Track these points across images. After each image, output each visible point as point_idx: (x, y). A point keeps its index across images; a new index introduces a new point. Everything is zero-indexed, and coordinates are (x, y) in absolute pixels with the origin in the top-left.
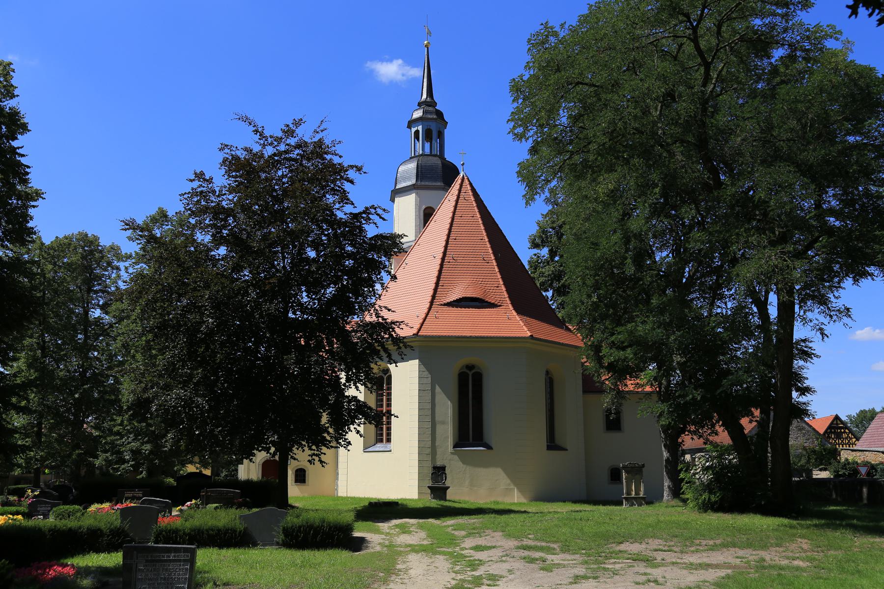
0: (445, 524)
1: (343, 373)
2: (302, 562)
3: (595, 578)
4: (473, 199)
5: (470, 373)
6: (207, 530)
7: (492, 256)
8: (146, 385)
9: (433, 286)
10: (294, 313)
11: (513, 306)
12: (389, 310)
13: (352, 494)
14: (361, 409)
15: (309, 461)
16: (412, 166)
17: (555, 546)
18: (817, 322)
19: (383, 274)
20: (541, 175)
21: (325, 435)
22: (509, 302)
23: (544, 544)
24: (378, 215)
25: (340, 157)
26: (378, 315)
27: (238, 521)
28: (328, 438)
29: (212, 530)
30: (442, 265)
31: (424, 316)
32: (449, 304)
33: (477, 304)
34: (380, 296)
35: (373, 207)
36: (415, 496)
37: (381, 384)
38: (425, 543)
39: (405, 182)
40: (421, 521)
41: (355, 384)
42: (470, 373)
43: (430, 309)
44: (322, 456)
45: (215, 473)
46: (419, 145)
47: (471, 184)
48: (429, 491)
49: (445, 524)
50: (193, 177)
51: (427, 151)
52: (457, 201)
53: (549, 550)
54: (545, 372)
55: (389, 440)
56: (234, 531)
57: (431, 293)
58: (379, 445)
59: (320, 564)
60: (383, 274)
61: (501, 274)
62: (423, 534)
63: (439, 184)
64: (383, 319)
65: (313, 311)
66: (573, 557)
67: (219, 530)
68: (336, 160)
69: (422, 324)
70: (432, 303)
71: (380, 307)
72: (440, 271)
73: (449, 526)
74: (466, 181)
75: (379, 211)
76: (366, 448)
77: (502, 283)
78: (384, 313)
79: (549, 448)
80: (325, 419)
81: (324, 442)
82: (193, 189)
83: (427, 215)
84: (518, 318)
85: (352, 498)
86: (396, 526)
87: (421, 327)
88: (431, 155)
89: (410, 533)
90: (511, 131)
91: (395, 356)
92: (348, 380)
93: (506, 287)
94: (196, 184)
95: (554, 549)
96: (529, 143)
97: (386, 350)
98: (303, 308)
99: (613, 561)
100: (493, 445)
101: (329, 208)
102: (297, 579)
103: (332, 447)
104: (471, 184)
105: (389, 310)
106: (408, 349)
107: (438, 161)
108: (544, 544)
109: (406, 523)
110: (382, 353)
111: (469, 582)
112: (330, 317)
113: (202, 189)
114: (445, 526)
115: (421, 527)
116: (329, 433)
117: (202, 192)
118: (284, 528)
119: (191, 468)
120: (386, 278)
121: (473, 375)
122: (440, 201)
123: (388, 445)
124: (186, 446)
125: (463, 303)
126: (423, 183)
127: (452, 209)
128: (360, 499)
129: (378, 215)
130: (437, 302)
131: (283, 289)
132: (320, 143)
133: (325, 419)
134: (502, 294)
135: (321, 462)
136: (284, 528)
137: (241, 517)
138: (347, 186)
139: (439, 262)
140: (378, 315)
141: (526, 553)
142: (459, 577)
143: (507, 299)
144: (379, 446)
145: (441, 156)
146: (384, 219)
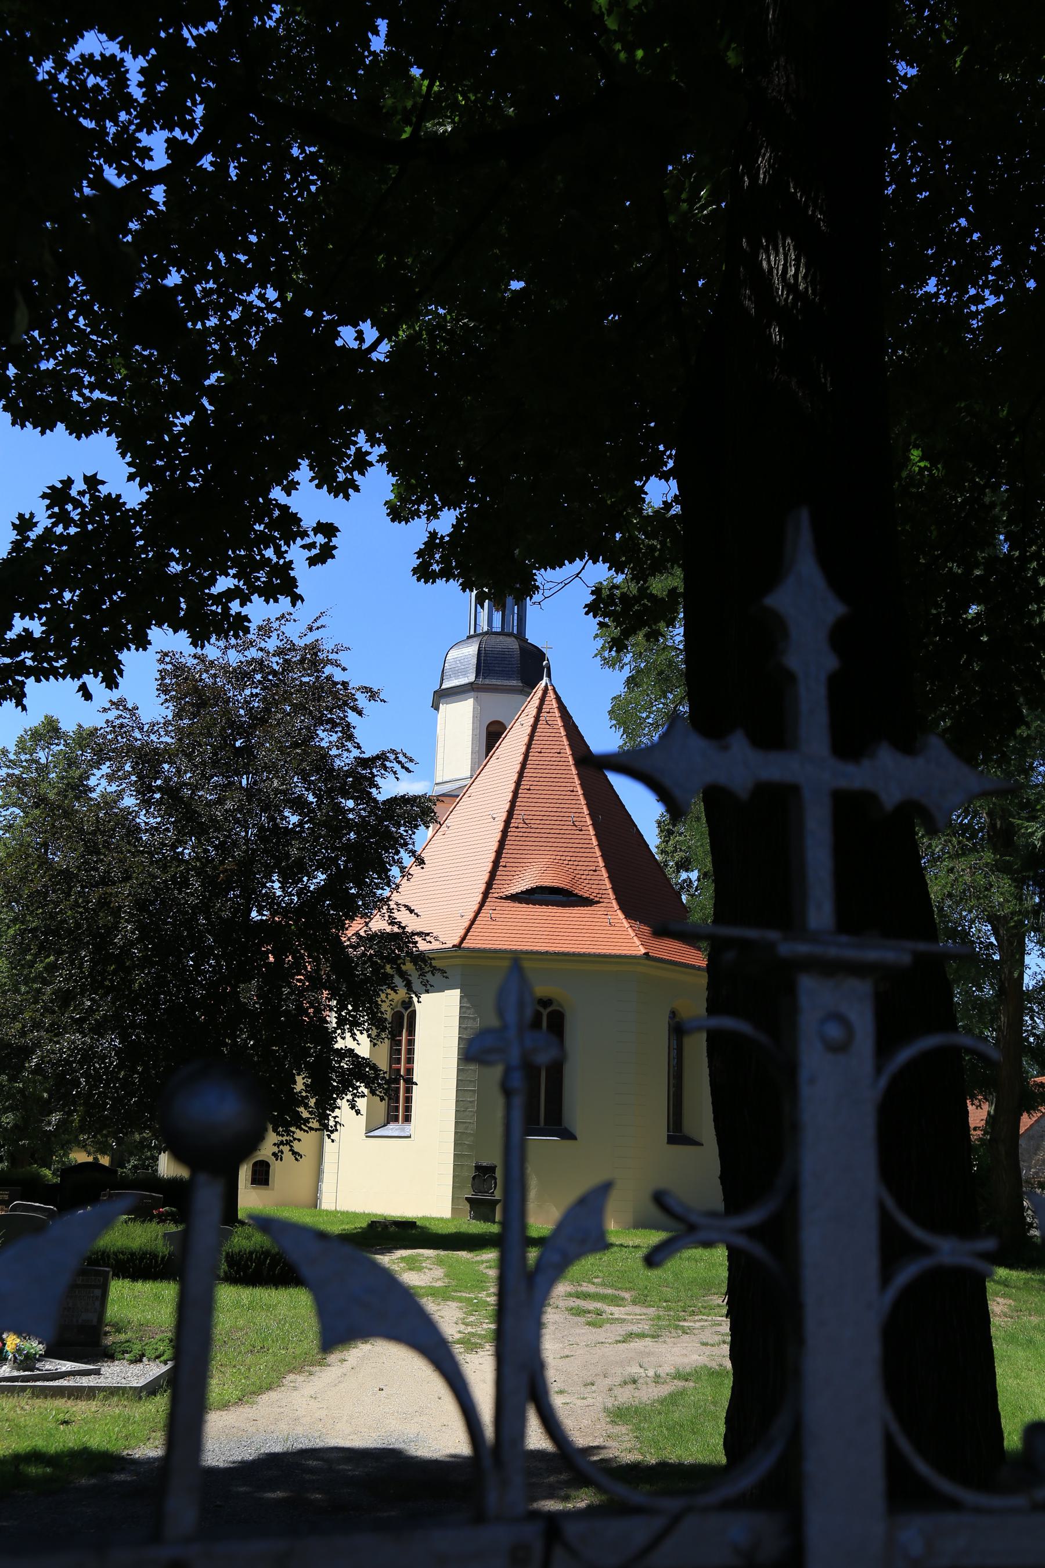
0: (478, 1258)
1: (334, 1014)
2: (251, 1302)
3: (653, 1337)
4: (560, 723)
5: (545, 1013)
6: (115, 1254)
7: (588, 819)
8: (24, 1026)
9: (489, 866)
10: (260, 913)
11: (619, 903)
12: (412, 911)
13: (343, 1207)
14: (361, 1070)
15: (274, 1154)
16: (471, 651)
17: (627, 1295)
18: (1038, 970)
19: (403, 854)
20: (648, 717)
21: (301, 1109)
22: (612, 896)
23: (610, 1291)
24: (399, 762)
25: (344, 669)
26: (392, 922)
27: (160, 1242)
28: (305, 1114)
29: (122, 1253)
30: (505, 833)
31: (471, 915)
32: (515, 898)
33: (560, 898)
34: (398, 886)
35: (393, 751)
36: (447, 1213)
37: (398, 1029)
38: (439, 1284)
39: (457, 677)
40: (442, 1253)
41: (351, 1031)
42: (545, 1013)
43: (482, 904)
44: (295, 1144)
45: (119, 1161)
46: (483, 615)
47: (558, 698)
48: (468, 1207)
49: (478, 1258)
50: (108, 705)
51: (497, 626)
52: (534, 727)
53: (616, 1301)
54: (667, 1014)
55: (407, 1119)
56: (154, 1256)
57: (486, 877)
58: (391, 1126)
59: (276, 1305)
60: (403, 854)
61: (601, 850)
62: (439, 1272)
63: (514, 683)
64: (400, 927)
65: (285, 912)
66: (644, 1310)
67: (133, 1254)
68: (339, 676)
69: (468, 930)
70: (486, 895)
71: (397, 904)
72: (502, 843)
73: (483, 1262)
74: (551, 693)
75: (401, 758)
76: (370, 1130)
77: (601, 864)
78: (402, 916)
79: (672, 1140)
80: (300, 1083)
81: (299, 1122)
82: (107, 721)
83: (492, 735)
84: (626, 924)
85: (342, 1213)
86: (403, 1259)
87: (466, 935)
88: (501, 633)
89: (420, 1269)
90: (599, 653)
91: (416, 984)
92: (341, 1021)
93: (608, 871)
94: (112, 714)
95: (623, 1299)
96: (626, 672)
97: (403, 975)
98: (271, 901)
99: (700, 1317)
100: (578, 1135)
101: (324, 756)
102: (241, 1323)
103: (311, 1129)
104: (558, 698)
105: (412, 911)
106: (438, 975)
107: (513, 644)
108: (610, 1291)
109: (419, 1255)
110: (397, 980)
111: (480, 1335)
112: (316, 922)
113: (121, 720)
114: (478, 1262)
115: (440, 1262)
116: (306, 1106)
117: (122, 726)
118: (228, 1254)
119: (80, 1157)
120: (408, 860)
121: (550, 1015)
122: (516, 711)
123: (406, 1126)
124: (82, 1120)
125: (537, 896)
126: (487, 682)
127: (526, 739)
128: (356, 1215)
129: (399, 762)
130: (495, 893)
131: (246, 878)
132: (314, 648)
133: (300, 1083)
134: (599, 881)
135: (294, 1153)
136: (228, 1254)
137: (165, 1235)
138: (352, 717)
139: (501, 826)
140: (392, 922)
141: (580, 1303)
142: (470, 1329)
143: (610, 891)
144: (392, 1129)
145: (521, 636)
146: (408, 770)
